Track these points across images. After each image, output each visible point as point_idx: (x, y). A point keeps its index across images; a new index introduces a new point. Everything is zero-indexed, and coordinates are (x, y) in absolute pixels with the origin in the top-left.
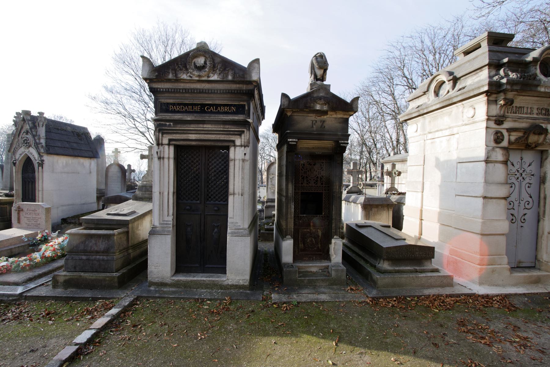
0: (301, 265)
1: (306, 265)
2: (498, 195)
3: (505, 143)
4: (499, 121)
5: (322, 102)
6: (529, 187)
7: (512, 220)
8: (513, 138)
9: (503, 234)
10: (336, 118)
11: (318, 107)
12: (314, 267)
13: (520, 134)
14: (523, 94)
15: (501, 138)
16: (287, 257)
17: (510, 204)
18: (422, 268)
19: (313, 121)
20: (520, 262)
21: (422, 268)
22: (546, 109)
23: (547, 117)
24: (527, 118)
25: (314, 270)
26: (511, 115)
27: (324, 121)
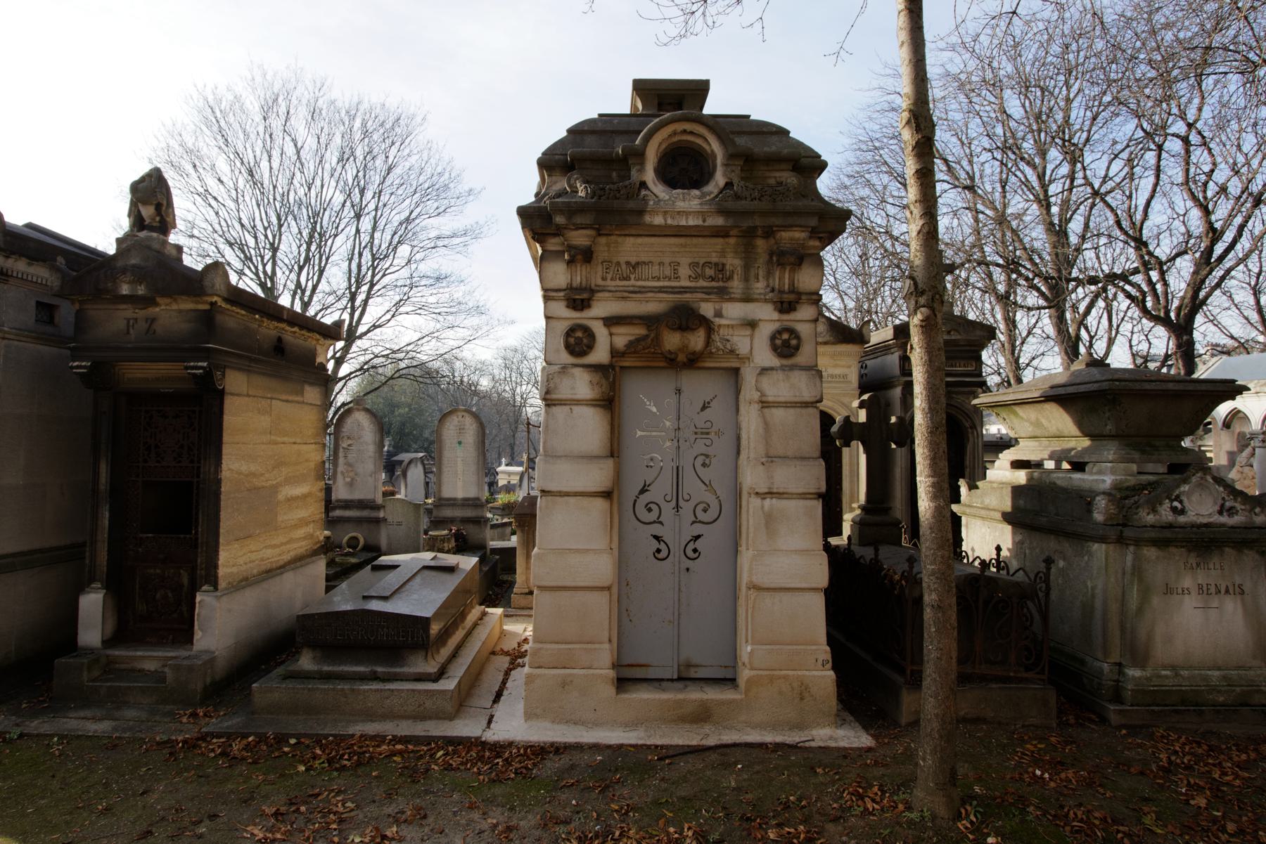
0: (117, 653)
1: (131, 653)
2: (794, 488)
3: (600, 354)
4: (578, 299)
5: (129, 277)
6: (704, 465)
7: (659, 551)
8: (620, 342)
9: (602, 589)
10: (180, 311)
11: (125, 290)
12: (150, 659)
13: (639, 331)
14: (633, 232)
15: (794, 342)
16: (91, 632)
17: (650, 510)
18: (398, 670)
19: (128, 320)
20: (689, 666)
21: (398, 670)
22: (716, 264)
23: (721, 284)
24: (661, 290)
25: (150, 666)
26: (613, 283)
27: (154, 320)
